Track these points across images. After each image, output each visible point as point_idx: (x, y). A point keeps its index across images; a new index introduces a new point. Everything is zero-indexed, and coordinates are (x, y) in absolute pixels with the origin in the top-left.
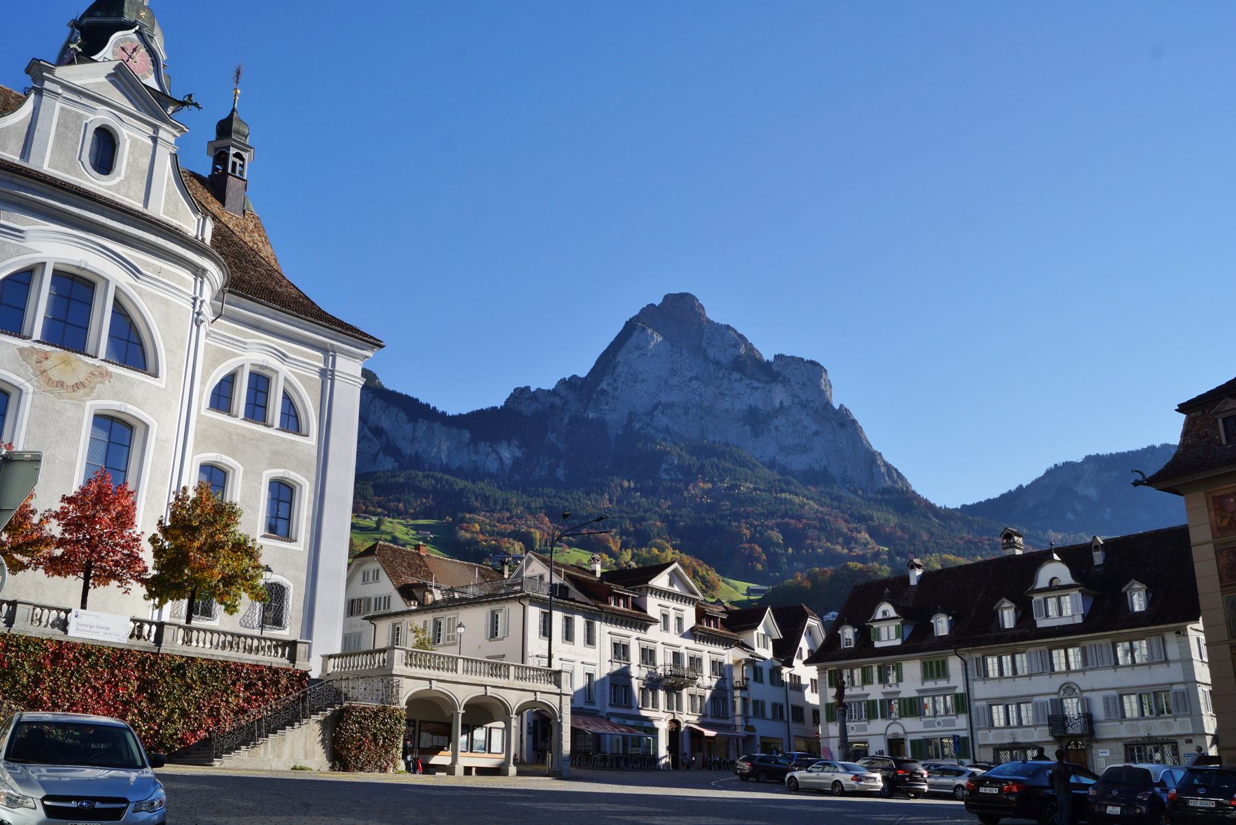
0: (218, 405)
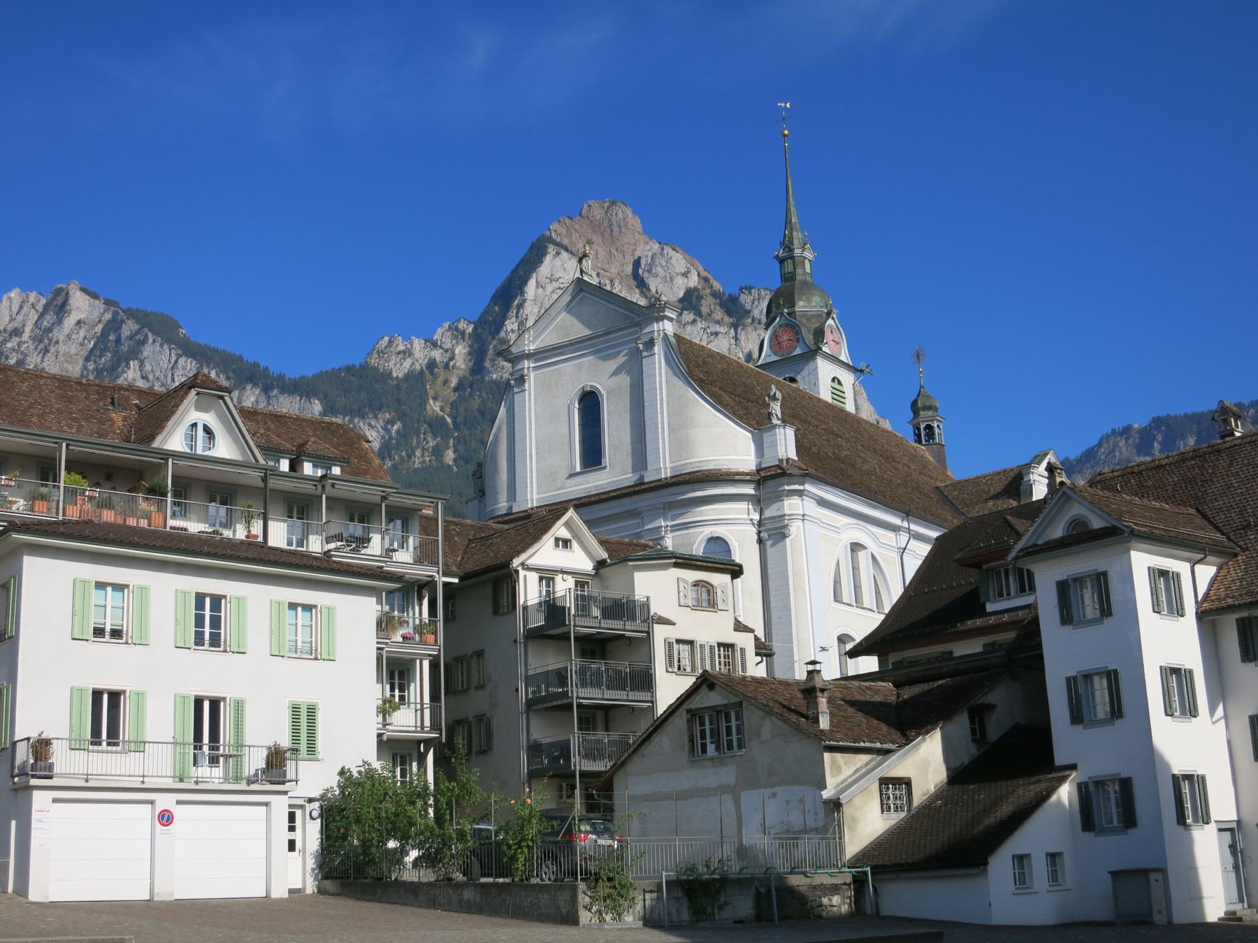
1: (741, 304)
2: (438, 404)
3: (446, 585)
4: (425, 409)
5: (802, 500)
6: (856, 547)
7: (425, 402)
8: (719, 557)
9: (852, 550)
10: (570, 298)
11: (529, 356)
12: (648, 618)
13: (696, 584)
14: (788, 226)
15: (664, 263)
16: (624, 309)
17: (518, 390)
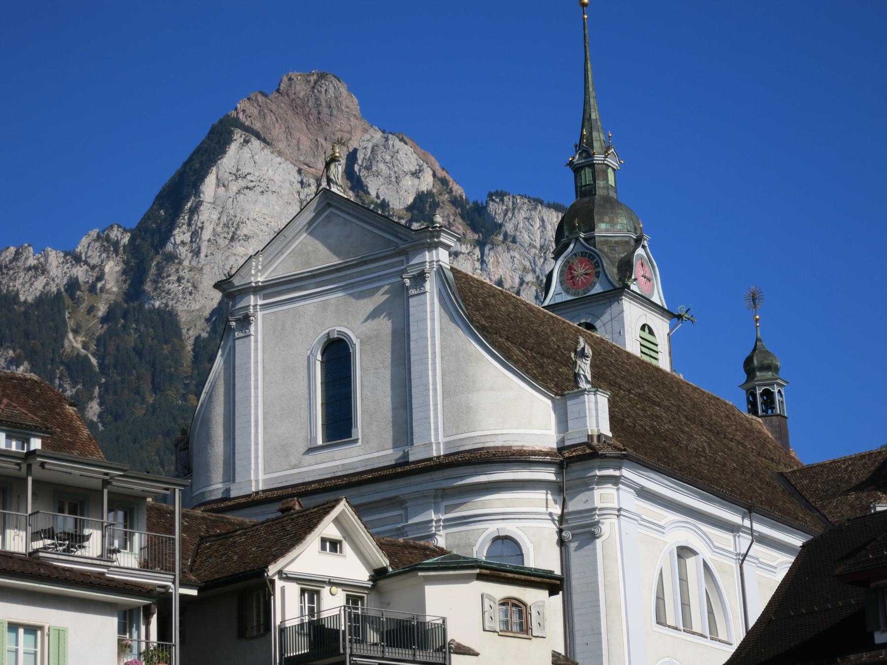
0: (581, 403)
1: (489, 215)
2: (79, 339)
3: (182, 596)
4: (63, 346)
5: (618, 489)
6: (684, 552)
7: (64, 336)
8: (509, 563)
9: (679, 556)
10: (313, 214)
11: (257, 290)
12: (444, 646)
13: (505, 602)
14: (586, 123)
15: (388, 158)
16: (385, 231)
17: (241, 335)
